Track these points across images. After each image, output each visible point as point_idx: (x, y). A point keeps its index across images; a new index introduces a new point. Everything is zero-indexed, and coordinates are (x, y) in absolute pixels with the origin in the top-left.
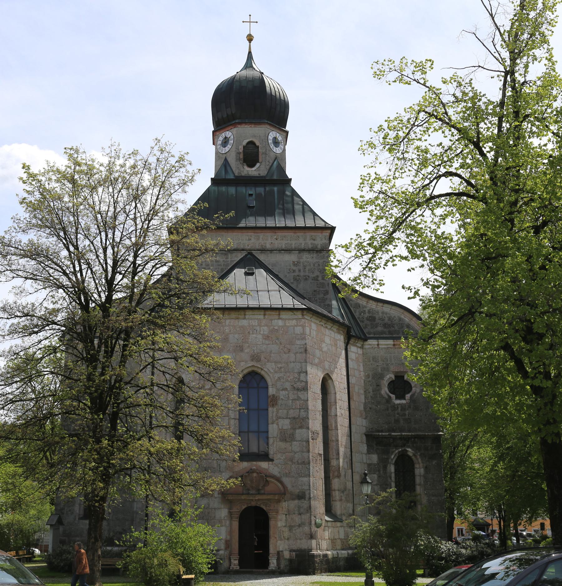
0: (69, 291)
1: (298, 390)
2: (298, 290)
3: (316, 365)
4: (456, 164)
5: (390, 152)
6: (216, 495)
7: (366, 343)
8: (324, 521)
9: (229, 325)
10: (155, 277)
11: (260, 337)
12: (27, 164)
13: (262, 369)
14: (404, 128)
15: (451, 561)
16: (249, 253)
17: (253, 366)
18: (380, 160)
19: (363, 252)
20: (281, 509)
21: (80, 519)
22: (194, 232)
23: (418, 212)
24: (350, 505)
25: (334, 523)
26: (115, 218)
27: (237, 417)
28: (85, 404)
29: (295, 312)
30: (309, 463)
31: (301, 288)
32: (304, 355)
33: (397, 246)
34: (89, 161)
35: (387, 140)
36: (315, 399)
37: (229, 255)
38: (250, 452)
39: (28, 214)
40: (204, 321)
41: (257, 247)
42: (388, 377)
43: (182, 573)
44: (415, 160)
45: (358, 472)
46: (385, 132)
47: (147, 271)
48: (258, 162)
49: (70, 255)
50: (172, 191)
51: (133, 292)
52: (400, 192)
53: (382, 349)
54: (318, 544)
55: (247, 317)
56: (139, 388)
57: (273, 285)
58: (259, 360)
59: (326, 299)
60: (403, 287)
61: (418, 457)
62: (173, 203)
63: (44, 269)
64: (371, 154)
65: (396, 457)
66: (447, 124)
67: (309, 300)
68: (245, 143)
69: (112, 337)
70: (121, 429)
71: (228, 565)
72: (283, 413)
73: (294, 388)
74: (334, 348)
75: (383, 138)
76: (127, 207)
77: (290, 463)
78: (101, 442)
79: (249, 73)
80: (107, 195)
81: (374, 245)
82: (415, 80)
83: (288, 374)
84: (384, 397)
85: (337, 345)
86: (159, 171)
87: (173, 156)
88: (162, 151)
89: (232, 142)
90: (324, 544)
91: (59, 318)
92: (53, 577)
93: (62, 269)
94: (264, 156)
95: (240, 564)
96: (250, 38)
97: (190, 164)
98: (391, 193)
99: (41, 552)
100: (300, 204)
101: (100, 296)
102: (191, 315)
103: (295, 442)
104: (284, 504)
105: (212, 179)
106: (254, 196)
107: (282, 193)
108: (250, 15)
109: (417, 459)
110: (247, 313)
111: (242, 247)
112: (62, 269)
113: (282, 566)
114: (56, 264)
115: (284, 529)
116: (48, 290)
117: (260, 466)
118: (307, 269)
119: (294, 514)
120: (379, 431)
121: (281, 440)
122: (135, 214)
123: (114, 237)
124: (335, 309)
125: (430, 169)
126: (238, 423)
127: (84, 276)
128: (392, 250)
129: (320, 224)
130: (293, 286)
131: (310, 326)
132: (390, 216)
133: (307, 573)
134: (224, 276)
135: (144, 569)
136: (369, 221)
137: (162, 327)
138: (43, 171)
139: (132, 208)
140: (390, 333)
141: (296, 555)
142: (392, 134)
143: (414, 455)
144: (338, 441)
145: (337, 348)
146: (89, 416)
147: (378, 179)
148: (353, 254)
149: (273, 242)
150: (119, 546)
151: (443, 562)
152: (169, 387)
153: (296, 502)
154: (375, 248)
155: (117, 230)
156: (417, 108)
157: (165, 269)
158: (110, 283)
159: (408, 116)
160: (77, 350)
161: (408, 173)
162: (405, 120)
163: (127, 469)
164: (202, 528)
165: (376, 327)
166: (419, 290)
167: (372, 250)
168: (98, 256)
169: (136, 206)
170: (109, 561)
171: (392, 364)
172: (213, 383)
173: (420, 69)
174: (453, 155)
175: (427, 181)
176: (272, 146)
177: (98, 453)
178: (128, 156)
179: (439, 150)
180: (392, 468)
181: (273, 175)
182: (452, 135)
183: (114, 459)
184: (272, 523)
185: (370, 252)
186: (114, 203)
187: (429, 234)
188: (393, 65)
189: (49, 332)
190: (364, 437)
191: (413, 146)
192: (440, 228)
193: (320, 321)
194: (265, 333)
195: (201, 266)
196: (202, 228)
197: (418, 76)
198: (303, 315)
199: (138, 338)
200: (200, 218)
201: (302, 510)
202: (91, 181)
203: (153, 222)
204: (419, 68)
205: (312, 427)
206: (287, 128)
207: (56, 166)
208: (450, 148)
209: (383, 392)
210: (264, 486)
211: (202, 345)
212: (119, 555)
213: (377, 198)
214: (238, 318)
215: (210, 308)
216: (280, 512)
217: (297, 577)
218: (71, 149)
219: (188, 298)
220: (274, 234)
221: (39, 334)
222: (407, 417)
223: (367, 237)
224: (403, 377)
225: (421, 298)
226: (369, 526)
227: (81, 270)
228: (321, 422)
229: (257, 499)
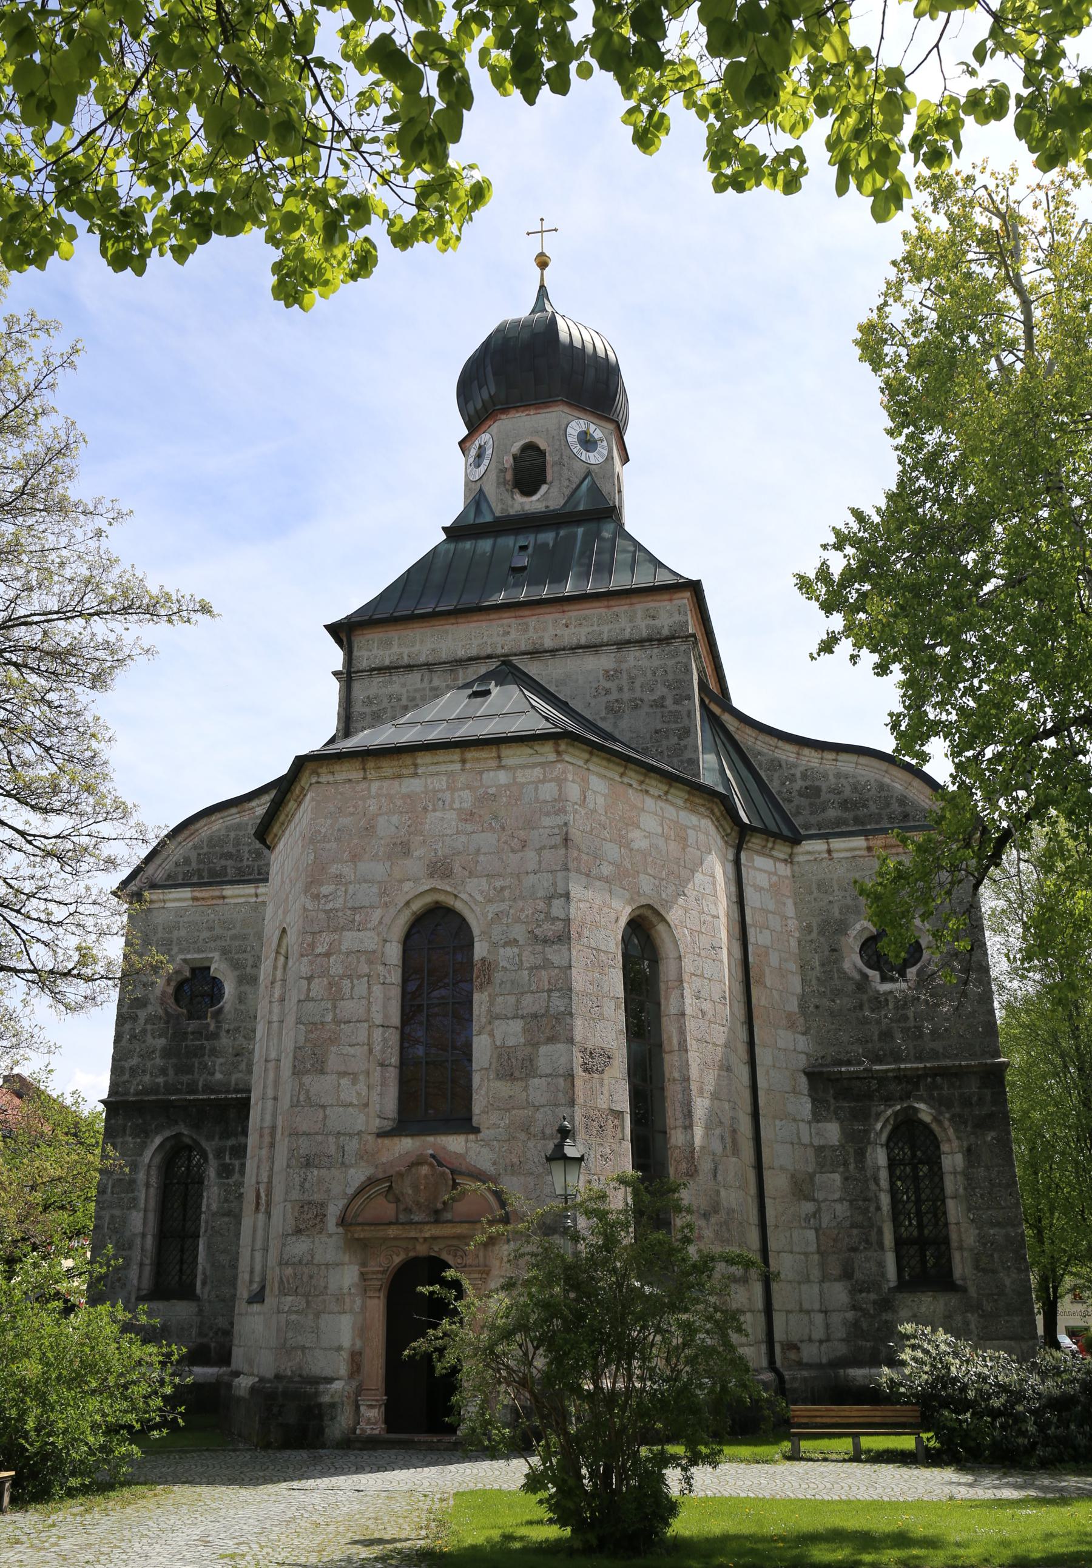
1: (545, 941)
7: (799, 849)
11: (451, 815)
16: (504, 663)
17: (433, 890)
20: (497, 1263)
32: (562, 851)
41: (523, 648)
42: (858, 927)
53: (840, 860)
59: (685, 747)
61: (947, 1123)
65: (889, 1128)
68: (516, 448)
72: (505, 1003)
73: (536, 937)
77: (523, 1136)
83: (521, 903)
84: (849, 978)
94: (556, 468)
96: (543, 262)
103: (536, 1081)
106: (530, 550)
109: (945, 1130)
110: (419, 761)
117: (444, 1148)
118: (637, 684)
120: (841, 1063)
121: (499, 1077)
131: (585, 780)
140: (857, 820)
143: (935, 1119)
144: (687, 1079)
149: (558, 632)
151: (968, 1415)
165: (824, 810)
180: (880, 1157)
181: (578, 503)
190: (803, 1080)
194: (465, 805)
198: (558, 753)
205: (586, 1038)
209: (847, 965)
214: (399, 777)
220: (560, 615)
222: (911, 1023)
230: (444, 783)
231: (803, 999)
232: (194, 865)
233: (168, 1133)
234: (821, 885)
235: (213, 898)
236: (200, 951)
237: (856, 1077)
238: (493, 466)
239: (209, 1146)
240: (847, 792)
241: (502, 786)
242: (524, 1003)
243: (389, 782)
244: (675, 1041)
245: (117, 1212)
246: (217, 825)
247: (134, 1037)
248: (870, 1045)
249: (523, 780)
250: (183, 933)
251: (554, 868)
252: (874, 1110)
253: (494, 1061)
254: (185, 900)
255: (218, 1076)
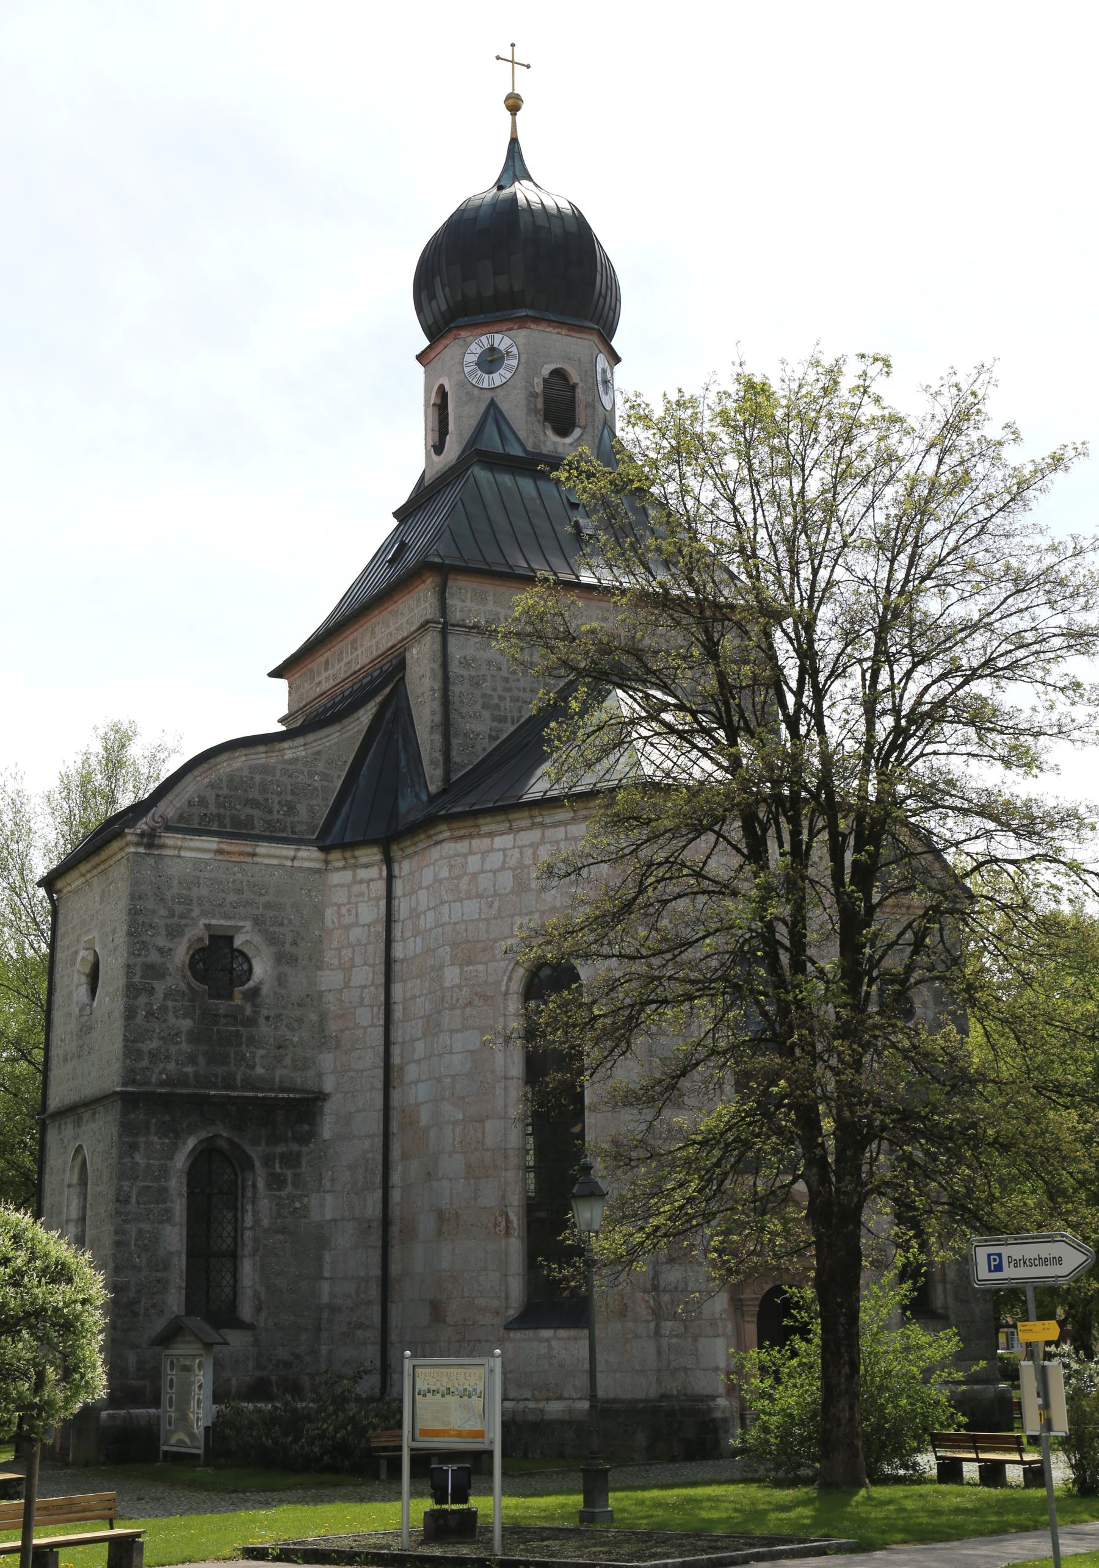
68: (546, 371)
89: (515, 363)
94: (589, 411)
96: (514, 104)
108: (513, 45)
224: (231, 939)
232: (212, 809)
233: (203, 1134)
235: (241, 854)
236: (227, 917)
239: (255, 1153)
245: (146, 1226)
246: (239, 762)
247: (150, 1014)
250: (204, 891)
254: (208, 851)
255: (259, 1070)
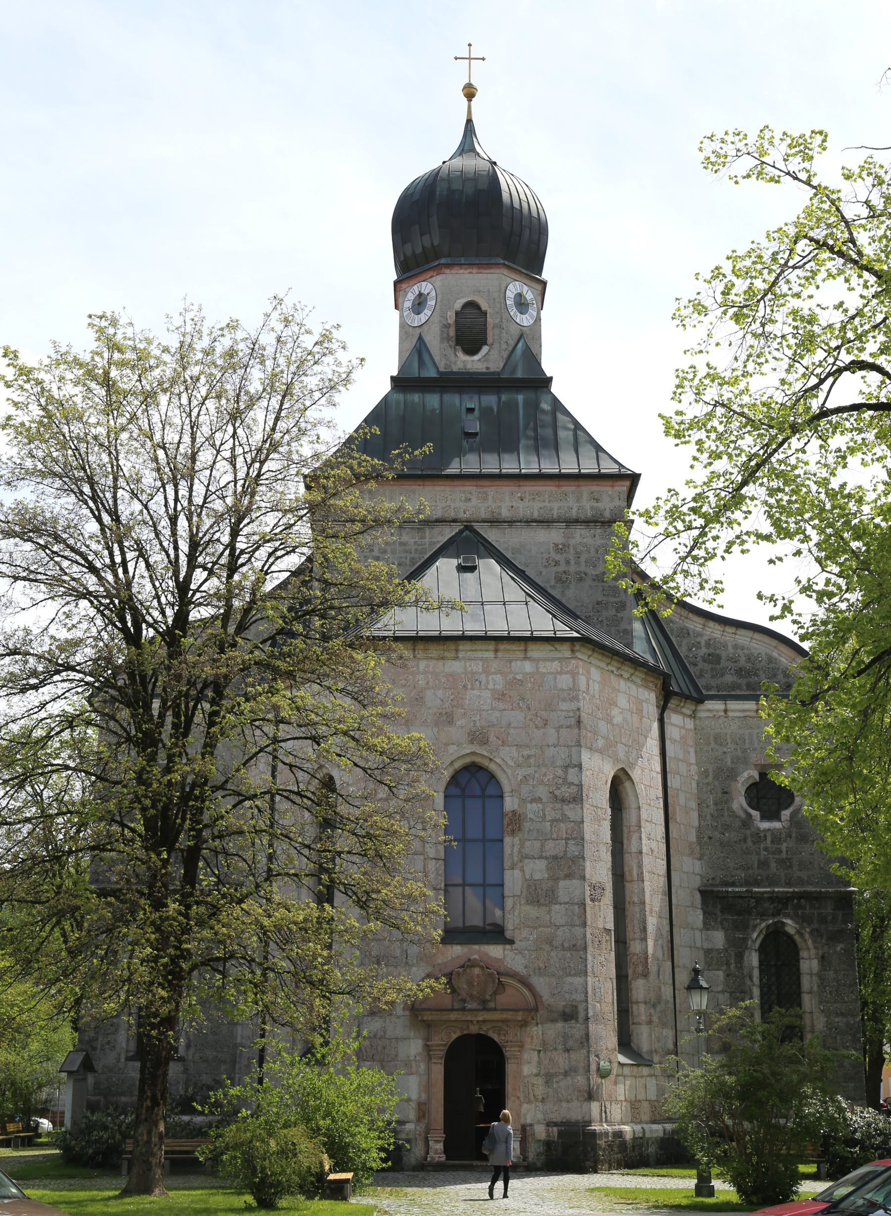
0: (101, 604)
1: (563, 800)
2: (564, 601)
3: (600, 751)
4: (872, 346)
5: (737, 322)
6: (399, 1011)
7: (702, 707)
8: (615, 1065)
9: (425, 672)
10: (275, 575)
11: (487, 694)
12: (13, 349)
13: (491, 760)
14: (766, 271)
15: (873, 1147)
16: (467, 528)
17: (473, 753)
18: (716, 338)
19: (680, 526)
20: (529, 1040)
21: (128, 1059)
22: (352, 485)
23: (795, 443)
24: (669, 1033)
25: (635, 1069)
26: (193, 458)
27: (442, 855)
28: (133, 830)
29: (557, 646)
30: (585, 948)
31: (569, 597)
32: (576, 731)
33: (750, 512)
34: (141, 341)
35: (732, 297)
36: (598, 820)
37: (427, 531)
38: (467, 924)
39: (16, 450)
40: (372, 664)
41: (483, 515)
42: (745, 775)
43: (327, 1168)
44: (789, 337)
45: (684, 967)
46: (725, 280)
47: (258, 565)
48: (486, 344)
49: (102, 530)
50: (308, 403)
51: (229, 606)
52: (758, 402)
53: (734, 718)
54: (603, 1111)
55: (461, 655)
56: (242, 797)
57: (515, 591)
58: (484, 742)
60: (760, 596)
61: (807, 936)
62: (309, 427)
63: (52, 559)
64: (698, 325)
65: (762, 937)
66: (855, 262)
67: (587, 620)
68: (458, 305)
69: (187, 695)
70: (206, 880)
71: (423, 1153)
72: (533, 846)
73: (556, 797)
74: (636, 718)
75: (723, 293)
76: (218, 436)
77: (547, 948)
78: (166, 906)
79: (467, 163)
80: (177, 411)
81: (703, 510)
82: (788, 173)
83: (544, 770)
85: (642, 711)
86: (282, 361)
87: (308, 332)
88: (287, 322)
89: (433, 303)
90: (616, 1111)
91: (79, 658)
92: (71, 1177)
93: (86, 560)
94: (496, 331)
95: (447, 1150)
96: (470, 93)
97: (344, 348)
98: (741, 406)
99: (54, 1124)
100: (568, 429)
101: (163, 613)
102: (346, 650)
104: (536, 1031)
105: (392, 378)
106: (476, 412)
107: (533, 407)
108: (470, 45)
110: (461, 647)
111: (452, 515)
112: (86, 560)
113: (531, 1156)
114: (73, 550)
115: (534, 1080)
116: (60, 601)
117: (487, 954)
118: (582, 559)
119: (555, 1049)
120: (727, 884)
121: (529, 902)
122: (233, 449)
123: (191, 495)
124: (640, 638)
125: (820, 355)
126: (443, 868)
127: (131, 574)
128: (741, 520)
129: (608, 468)
130: (557, 595)
131: (588, 672)
132: (737, 452)
133: (581, 1169)
134: (416, 573)
135: (249, 1162)
136: (695, 463)
137: (290, 675)
138: (47, 361)
139: (227, 437)
140: (749, 686)
141: (560, 1133)
142: (741, 285)
143: (798, 932)
144: (644, 903)
145: (642, 717)
146: (141, 853)
147: (713, 376)
148: (661, 529)
149: (514, 504)
150: (202, 1113)
152: (302, 796)
153: (560, 1025)
154: (704, 516)
155: (196, 481)
156: (792, 231)
157: (294, 561)
158: (183, 587)
159: (774, 247)
160: (117, 721)
161: (773, 363)
162: (767, 256)
163: (218, 959)
164: (370, 1076)
165: (722, 675)
166: (791, 602)
167: (700, 522)
168: (157, 534)
169: (235, 433)
170: (183, 1145)
171: (755, 749)
172: (390, 788)
173: (801, 151)
174: (867, 327)
175: (814, 381)
176: (513, 311)
177: (158, 929)
178: (220, 333)
179: (837, 318)
180: (753, 959)
181: (514, 371)
182: (866, 286)
183: (188, 941)
184: (510, 1068)
185: (694, 524)
186: (192, 428)
187: (814, 488)
188: (744, 142)
189: (60, 685)
190: (698, 896)
191: (785, 310)
192: (835, 475)
193: (608, 664)
194: (498, 687)
195: (368, 552)
196: (368, 477)
197: (795, 164)
198: (573, 651)
199: (238, 699)
200: (364, 457)
201: (571, 1043)
202: (144, 382)
203: (268, 465)
204: (797, 149)
205: (591, 876)
206: (545, 275)
207: (74, 351)
208: (859, 313)
209: (735, 806)
210: (495, 993)
211: (365, 713)
212: (200, 1133)
213: (710, 416)
214: (443, 658)
215: (384, 638)
216: (528, 1046)
217: (561, 1177)
218: (101, 317)
219: (340, 617)
220: (516, 489)
221: (41, 690)
222: (784, 855)
223: (689, 493)
225: (795, 617)
226: (702, 1077)
227: (124, 563)
228: (609, 864)
229: (481, 1019)
230: (480, 667)
231: (699, 830)
234: (717, 738)
237: (739, 896)
238: (436, 318)
240: (742, 662)
241: (527, 674)
242: (547, 847)
243: (434, 661)
244: (635, 873)
248: (751, 871)
249: (544, 671)
251: (570, 743)
252: (751, 923)
253: (524, 890)
